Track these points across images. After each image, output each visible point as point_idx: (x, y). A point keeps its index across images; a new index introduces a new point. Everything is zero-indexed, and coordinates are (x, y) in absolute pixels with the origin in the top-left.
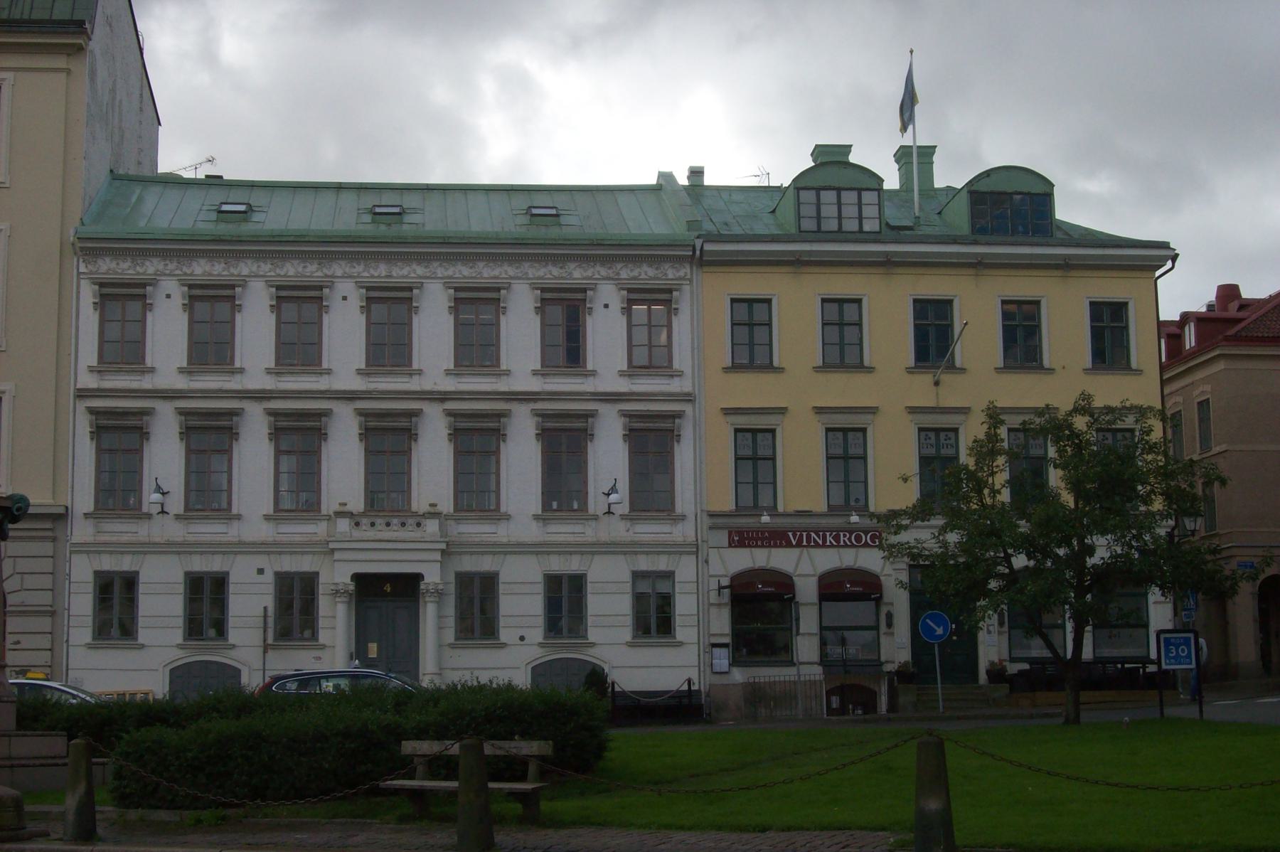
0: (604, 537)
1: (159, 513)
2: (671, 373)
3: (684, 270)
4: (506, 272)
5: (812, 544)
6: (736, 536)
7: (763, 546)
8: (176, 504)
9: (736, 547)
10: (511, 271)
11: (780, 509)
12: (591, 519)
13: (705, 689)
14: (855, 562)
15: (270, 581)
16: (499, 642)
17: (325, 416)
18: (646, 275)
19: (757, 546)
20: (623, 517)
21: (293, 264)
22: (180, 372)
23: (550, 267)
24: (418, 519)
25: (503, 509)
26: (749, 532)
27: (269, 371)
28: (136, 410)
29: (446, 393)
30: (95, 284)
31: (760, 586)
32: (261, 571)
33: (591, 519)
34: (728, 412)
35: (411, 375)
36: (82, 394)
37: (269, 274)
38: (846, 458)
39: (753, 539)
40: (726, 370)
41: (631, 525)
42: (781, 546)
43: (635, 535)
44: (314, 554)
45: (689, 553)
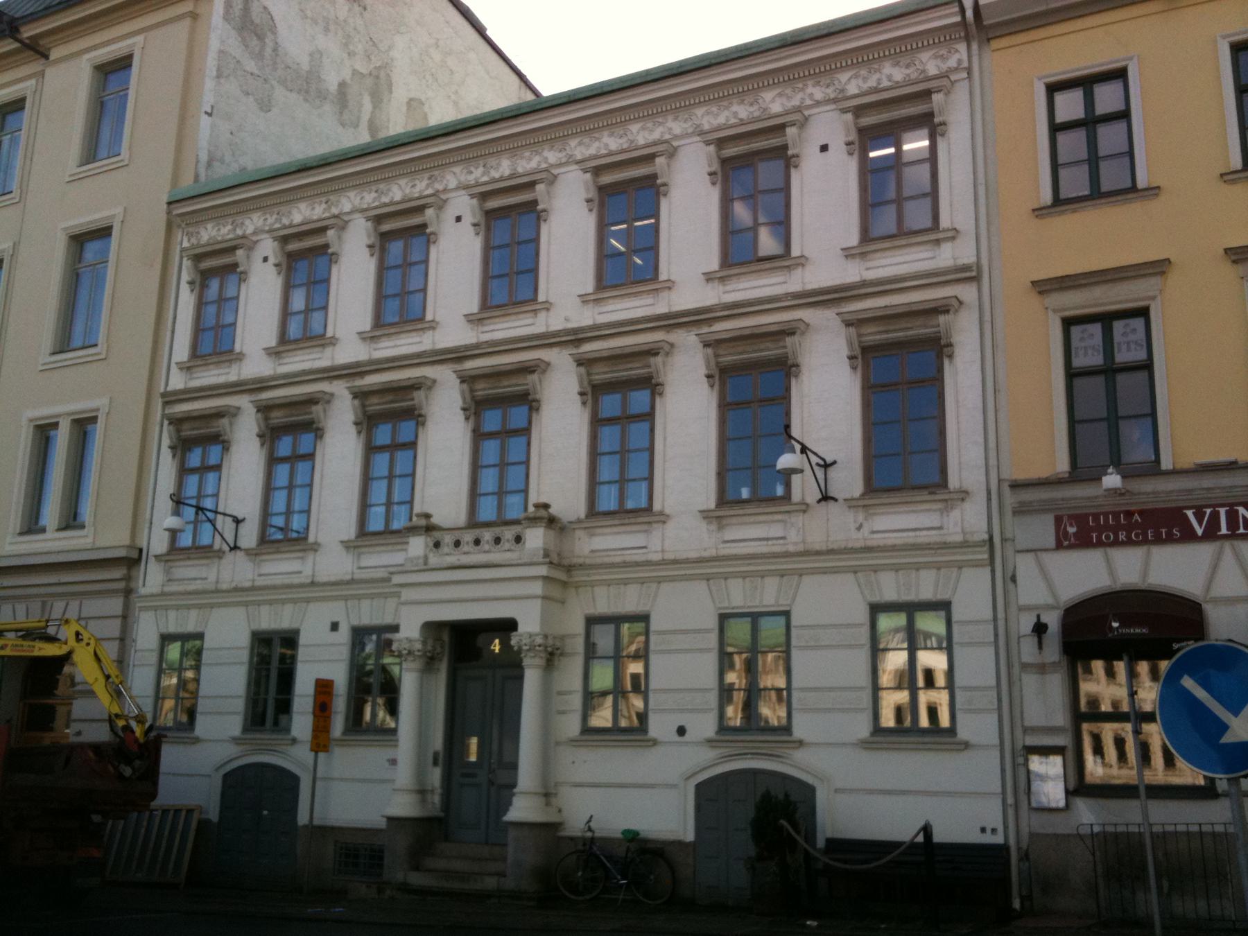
0: (817, 540)
1: (819, 501)
2: (934, 232)
3: (957, 56)
4: (735, 114)
5: (1242, 531)
6: (1071, 525)
7: (1129, 542)
8: (249, 536)
9: (1071, 547)
10: (552, 156)
11: (1166, 464)
12: (797, 511)
13: (1018, 842)
14: (1145, 574)
15: (244, 645)
16: (645, 738)
17: (792, 333)
18: (890, 81)
19: (1116, 543)
20: (851, 503)
21: (454, 173)
22: (583, 302)
23: (735, 108)
24: (516, 529)
25: (657, 506)
26: (1119, 513)
27: (709, 277)
28: (509, 367)
29: (261, 380)
30: (708, 143)
31: (1115, 625)
32: (335, 627)
33: (797, 511)
34: (1044, 287)
35: (937, 242)
36: (170, 398)
37: (324, 216)
38: (1110, 370)
39: (1107, 527)
40: (1040, 212)
41: (866, 519)
42: (1170, 539)
43: (875, 536)
44: (271, 604)
45: (976, 564)
